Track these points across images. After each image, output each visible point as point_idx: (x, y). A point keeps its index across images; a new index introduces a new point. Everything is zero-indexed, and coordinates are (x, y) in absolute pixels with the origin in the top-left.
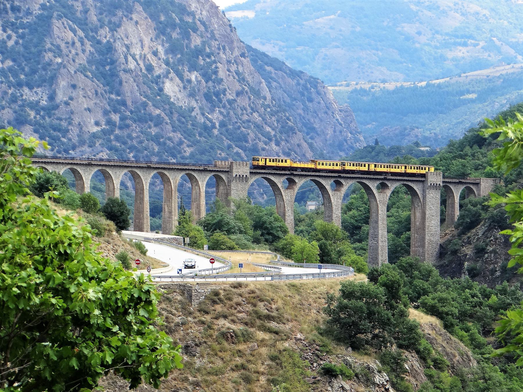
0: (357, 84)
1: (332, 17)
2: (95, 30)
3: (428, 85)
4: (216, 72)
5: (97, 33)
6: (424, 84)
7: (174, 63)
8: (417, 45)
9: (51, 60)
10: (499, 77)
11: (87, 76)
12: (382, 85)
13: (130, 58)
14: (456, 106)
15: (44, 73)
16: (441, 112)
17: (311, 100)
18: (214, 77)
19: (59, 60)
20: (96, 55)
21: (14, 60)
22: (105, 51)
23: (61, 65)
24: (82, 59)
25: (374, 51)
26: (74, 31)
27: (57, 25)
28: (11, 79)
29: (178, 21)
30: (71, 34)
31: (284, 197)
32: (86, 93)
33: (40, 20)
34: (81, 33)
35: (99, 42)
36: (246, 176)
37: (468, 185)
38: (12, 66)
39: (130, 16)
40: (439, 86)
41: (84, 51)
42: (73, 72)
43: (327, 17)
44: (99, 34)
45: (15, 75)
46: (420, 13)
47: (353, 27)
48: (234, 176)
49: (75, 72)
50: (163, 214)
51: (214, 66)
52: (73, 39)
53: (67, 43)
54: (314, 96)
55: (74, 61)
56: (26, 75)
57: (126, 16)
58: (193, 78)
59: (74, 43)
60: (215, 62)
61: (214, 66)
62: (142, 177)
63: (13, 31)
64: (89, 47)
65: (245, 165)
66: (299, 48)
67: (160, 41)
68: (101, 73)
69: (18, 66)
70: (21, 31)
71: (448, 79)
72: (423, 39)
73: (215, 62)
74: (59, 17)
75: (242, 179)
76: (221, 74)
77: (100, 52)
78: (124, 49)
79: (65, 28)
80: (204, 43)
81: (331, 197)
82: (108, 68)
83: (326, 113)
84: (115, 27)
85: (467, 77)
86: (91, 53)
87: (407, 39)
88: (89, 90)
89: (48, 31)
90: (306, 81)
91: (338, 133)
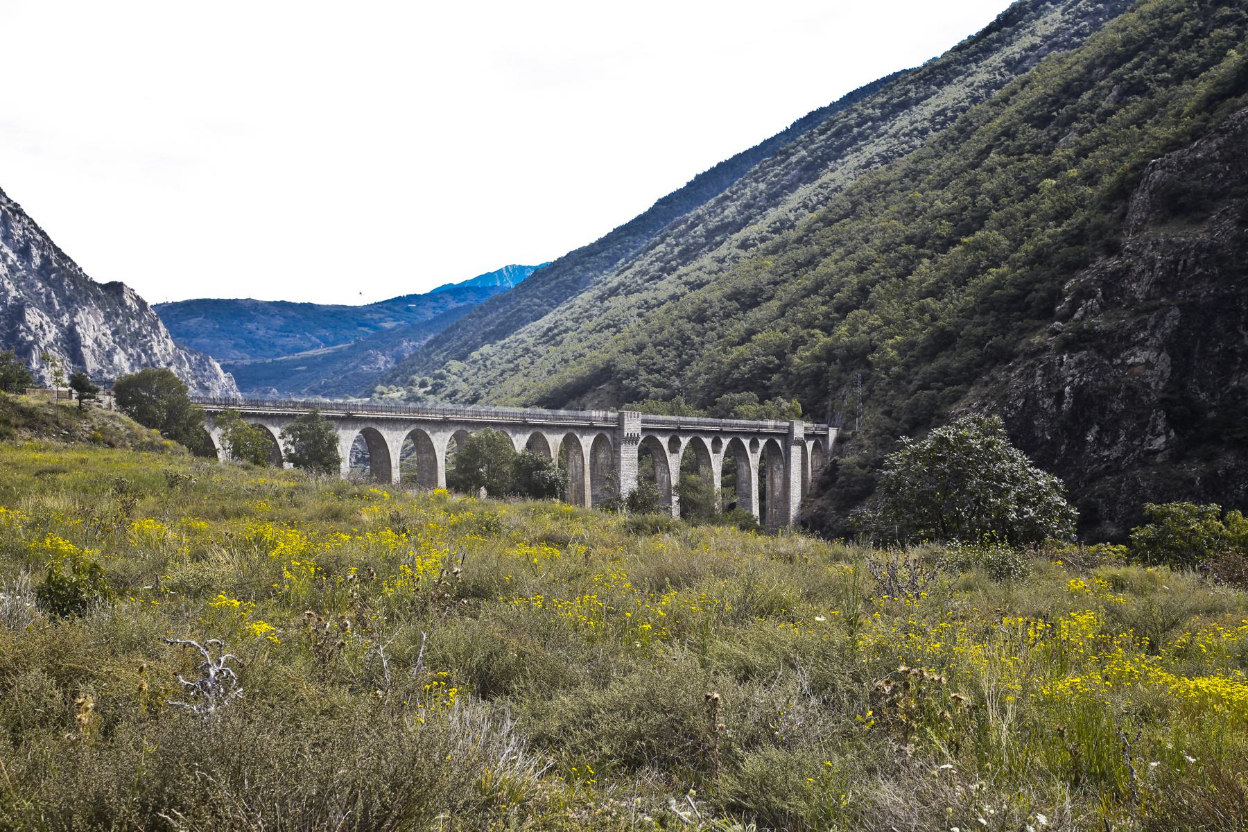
3: (273, 361)
6: (270, 360)
13: (87, 338)
17: (205, 370)
19: (31, 338)
24: (50, 337)
34: (48, 319)
35: (62, 325)
40: (281, 361)
59: (41, 326)
64: (54, 330)
72: (261, 333)
73: (150, 341)
74: (29, 306)
75: (632, 439)
76: (156, 350)
84: (73, 316)
87: (250, 333)
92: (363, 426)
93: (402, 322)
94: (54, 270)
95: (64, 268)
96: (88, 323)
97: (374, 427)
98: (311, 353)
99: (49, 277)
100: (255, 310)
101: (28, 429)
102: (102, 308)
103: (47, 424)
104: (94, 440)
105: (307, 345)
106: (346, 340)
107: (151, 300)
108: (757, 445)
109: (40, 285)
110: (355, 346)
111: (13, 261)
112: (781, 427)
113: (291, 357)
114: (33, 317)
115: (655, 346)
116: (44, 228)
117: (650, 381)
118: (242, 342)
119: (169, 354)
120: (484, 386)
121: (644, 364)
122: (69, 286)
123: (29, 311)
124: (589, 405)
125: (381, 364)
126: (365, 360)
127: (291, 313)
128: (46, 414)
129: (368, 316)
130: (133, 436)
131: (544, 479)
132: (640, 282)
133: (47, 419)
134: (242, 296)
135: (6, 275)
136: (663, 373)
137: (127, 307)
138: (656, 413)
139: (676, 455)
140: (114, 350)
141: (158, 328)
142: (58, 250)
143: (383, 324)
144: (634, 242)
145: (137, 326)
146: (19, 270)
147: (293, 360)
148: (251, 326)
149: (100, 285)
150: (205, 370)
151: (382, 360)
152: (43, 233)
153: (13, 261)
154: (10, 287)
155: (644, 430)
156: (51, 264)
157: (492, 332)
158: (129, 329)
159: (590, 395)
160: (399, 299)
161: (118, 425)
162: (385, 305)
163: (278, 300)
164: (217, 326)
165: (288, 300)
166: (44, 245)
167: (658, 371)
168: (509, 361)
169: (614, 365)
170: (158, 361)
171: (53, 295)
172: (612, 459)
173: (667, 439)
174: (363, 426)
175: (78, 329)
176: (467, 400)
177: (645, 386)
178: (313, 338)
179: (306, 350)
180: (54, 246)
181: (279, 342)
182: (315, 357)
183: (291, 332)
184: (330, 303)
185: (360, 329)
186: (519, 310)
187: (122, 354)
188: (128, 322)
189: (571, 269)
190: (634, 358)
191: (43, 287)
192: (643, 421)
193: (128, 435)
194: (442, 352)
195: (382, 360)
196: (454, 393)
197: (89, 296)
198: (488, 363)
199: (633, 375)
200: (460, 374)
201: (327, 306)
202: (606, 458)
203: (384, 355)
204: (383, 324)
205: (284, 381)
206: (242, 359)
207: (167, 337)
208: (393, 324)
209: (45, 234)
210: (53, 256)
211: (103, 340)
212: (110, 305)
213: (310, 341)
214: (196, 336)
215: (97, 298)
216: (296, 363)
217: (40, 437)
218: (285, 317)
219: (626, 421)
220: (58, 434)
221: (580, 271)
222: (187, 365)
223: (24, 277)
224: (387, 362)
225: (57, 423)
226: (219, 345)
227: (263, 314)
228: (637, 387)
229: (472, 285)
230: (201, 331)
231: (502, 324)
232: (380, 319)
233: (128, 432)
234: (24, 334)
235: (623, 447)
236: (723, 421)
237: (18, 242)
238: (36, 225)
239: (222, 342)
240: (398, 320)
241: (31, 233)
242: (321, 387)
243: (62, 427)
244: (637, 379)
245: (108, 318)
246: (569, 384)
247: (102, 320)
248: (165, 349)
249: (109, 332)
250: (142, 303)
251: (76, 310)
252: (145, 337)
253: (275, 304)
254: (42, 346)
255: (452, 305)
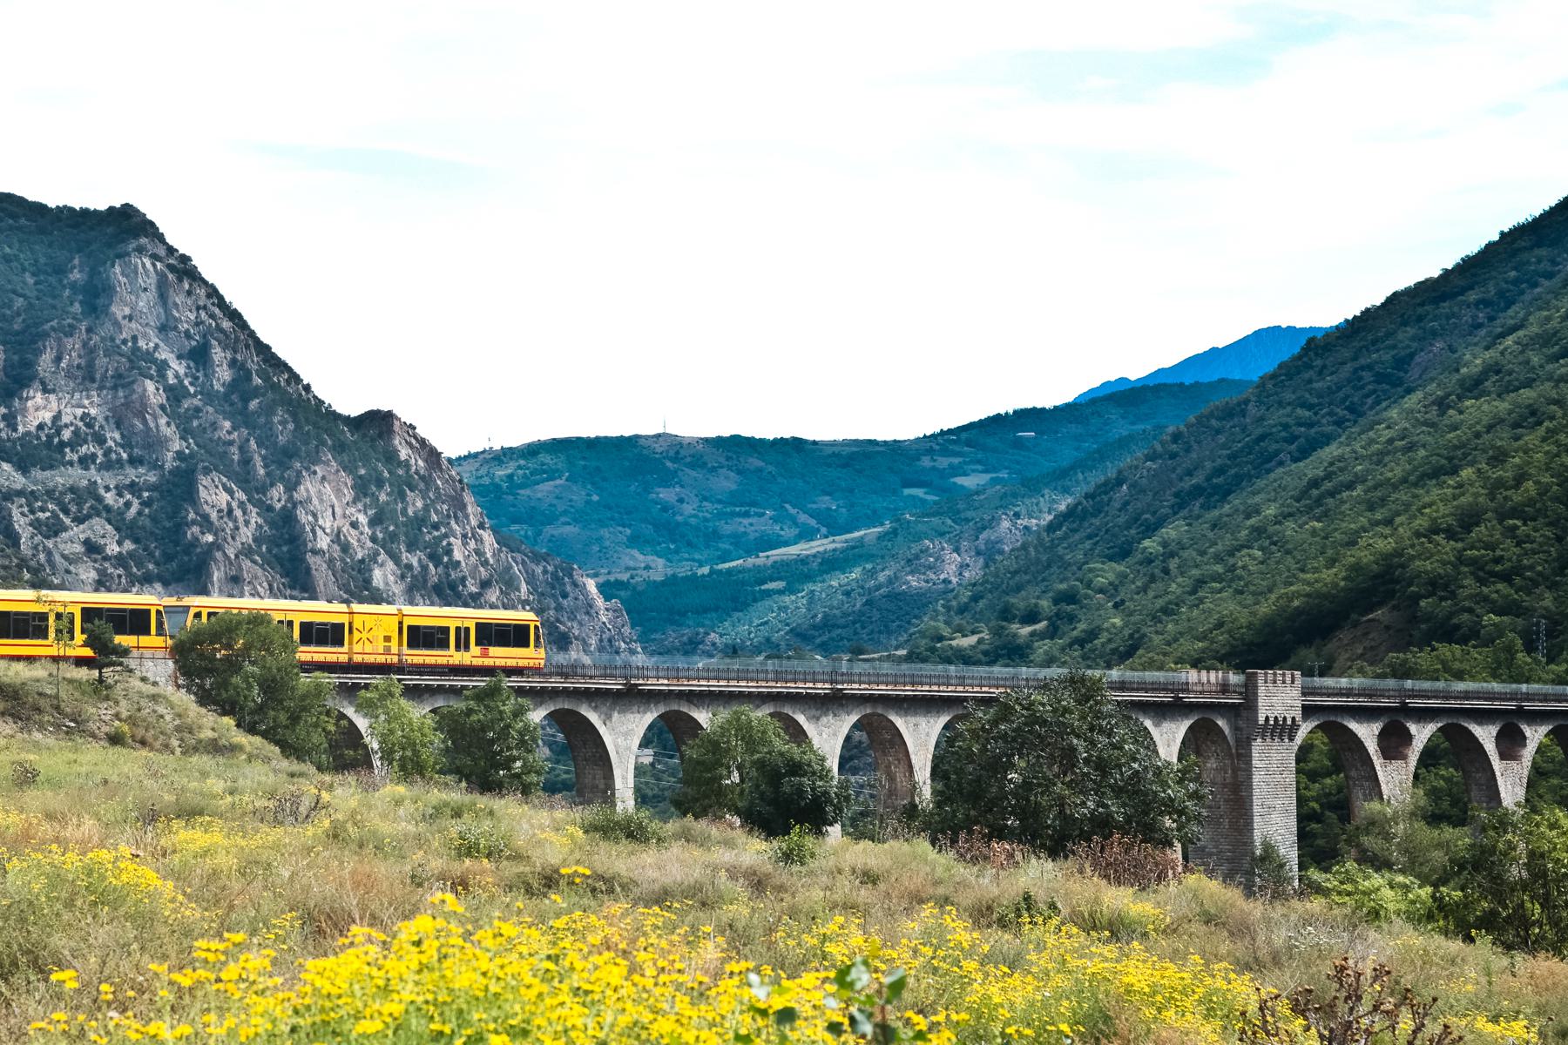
0: (609, 573)
1: (558, 482)
2: (263, 490)
3: (712, 572)
4: (449, 552)
5: (265, 495)
6: (706, 570)
7: (384, 539)
8: (679, 518)
9: (197, 539)
10: (814, 556)
11: (254, 562)
12: (645, 574)
13: (319, 532)
14: (755, 600)
15: (186, 558)
16: (736, 610)
17: (565, 596)
18: (446, 559)
19: (210, 538)
20: (266, 528)
21: (136, 541)
22: (281, 523)
23: (216, 546)
24: (246, 534)
25: (620, 529)
26: (230, 492)
27: (204, 483)
28: (135, 570)
29: (386, 474)
30: (224, 497)
31: (1384, 787)
32: (255, 588)
33: (175, 476)
34: (241, 495)
35: (270, 508)
36: (1293, 719)
37: (1332, 718)
38: (134, 550)
39: (313, 468)
40: (729, 572)
41: (247, 523)
42: (233, 557)
43: (551, 483)
44: (269, 496)
45: (139, 565)
46: (680, 473)
47: (588, 495)
48: (1261, 720)
49: (237, 556)
50: (827, 839)
51: (444, 543)
52: (229, 504)
53: (220, 511)
54: (569, 588)
55: (233, 538)
56: (157, 564)
57: (308, 469)
58: (415, 563)
59: (230, 511)
60: (446, 536)
61: (444, 543)
62: (602, 730)
63: (133, 495)
64: (255, 519)
65: (1288, 679)
66: (514, 527)
67: (360, 506)
68: (275, 556)
69: (144, 550)
70: (146, 494)
71: (741, 561)
72: (688, 509)
73: (446, 536)
74: (207, 471)
75: (1283, 730)
76: (458, 555)
77: (272, 524)
78: (310, 518)
79: (217, 487)
80: (426, 508)
81: (1500, 781)
82: (285, 549)
83: (588, 613)
84: (292, 487)
85: (768, 557)
86: (259, 527)
87: (665, 509)
88: (260, 585)
89: (191, 496)
90: (556, 567)
91: (606, 643)
92: (662, 709)
93: (1004, 474)
94: (256, 392)
95: (275, 387)
96: (321, 501)
97: (684, 709)
98: (794, 550)
99: (246, 408)
100: (676, 458)
101: (10, 720)
102: (349, 468)
103: (39, 710)
104: (115, 740)
105: (789, 532)
106: (873, 519)
107: (451, 446)
108: (1522, 740)
109: (227, 424)
110: (894, 532)
111: (177, 376)
112: (1382, 693)
113: (751, 561)
114: (214, 495)
115: (1501, 518)
116: (238, 305)
117: (1486, 599)
118: (648, 530)
119: (485, 563)
120: (1155, 619)
121: (1473, 562)
122: (283, 423)
123: (204, 481)
124: (1343, 658)
125: (950, 571)
126: (913, 564)
127: (755, 462)
128: (40, 694)
129: (926, 462)
130: (185, 729)
131: (800, 791)
132: (1535, 360)
133: (43, 703)
134: (648, 428)
135: (162, 407)
136: (1517, 580)
137: (400, 463)
138: (1459, 676)
139: (1399, 763)
140: (373, 557)
141: (463, 507)
142: (264, 350)
143: (960, 480)
144: (1554, 262)
145: (419, 504)
146: (187, 394)
147: (757, 568)
148: (666, 494)
149: (347, 420)
150: (565, 596)
151: (951, 561)
152: (235, 316)
153: (177, 376)
154: (168, 431)
155: (1308, 711)
156: (249, 378)
157: (1197, 491)
158: (404, 511)
159: (1344, 635)
160: (997, 419)
161: (161, 710)
162: (964, 436)
163: (726, 433)
164: (595, 498)
165: (746, 432)
166: (237, 340)
167: (1506, 577)
168: (1218, 559)
169: (1403, 566)
170: (464, 579)
171: (253, 444)
172: (1235, 771)
173: (1493, 730)
174: (662, 709)
175: (304, 517)
176: (1114, 651)
177: (1470, 611)
178: (803, 518)
179: (787, 544)
180: (258, 342)
181: (727, 528)
182: (803, 560)
183: (753, 504)
184: (840, 436)
185: (907, 491)
186: (1262, 438)
187: (390, 565)
188: (402, 496)
189: (1389, 335)
190: (1448, 547)
191: (234, 428)
192: (1306, 692)
193: (178, 729)
194: (1081, 541)
195: (951, 561)
196: (1092, 634)
197: (324, 443)
198: (1173, 564)
199: (1446, 587)
200: (1111, 590)
201: (834, 444)
202: (1223, 769)
203: (957, 550)
204: (960, 480)
205: (736, 615)
206: (647, 568)
207: (481, 526)
208: (983, 479)
209: (240, 316)
210: (253, 362)
211: (352, 537)
212: (366, 460)
213: (795, 523)
214: (551, 519)
215: (340, 448)
216: (762, 576)
217: (29, 732)
218: (739, 472)
219: (1261, 691)
220: (58, 727)
221: (1413, 339)
222: (524, 587)
223: (198, 410)
224: (964, 566)
225: (57, 708)
226: (600, 539)
227: (692, 466)
228: (1451, 615)
229: (1170, 381)
230: (561, 508)
231: (1220, 471)
232: (951, 466)
233: (177, 722)
234: (196, 529)
235: (1257, 746)
236: (1524, 687)
237: (188, 335)
238: (221, 298)
239: (604, 532)
240: (995, 470)
241: (212, 316)
242: (814, 627)
243: (66, 716)
244: (1453, 595)
245: (362, 489)
246: (1299, 612)
247: (349, 495)
248: (478, 552)
249: (363, 519)
250: (432, 455)
251: (299, 473)
252: (436, 527)
253: (719, 443)
254: (231, 553)
255: (1121, 429)
